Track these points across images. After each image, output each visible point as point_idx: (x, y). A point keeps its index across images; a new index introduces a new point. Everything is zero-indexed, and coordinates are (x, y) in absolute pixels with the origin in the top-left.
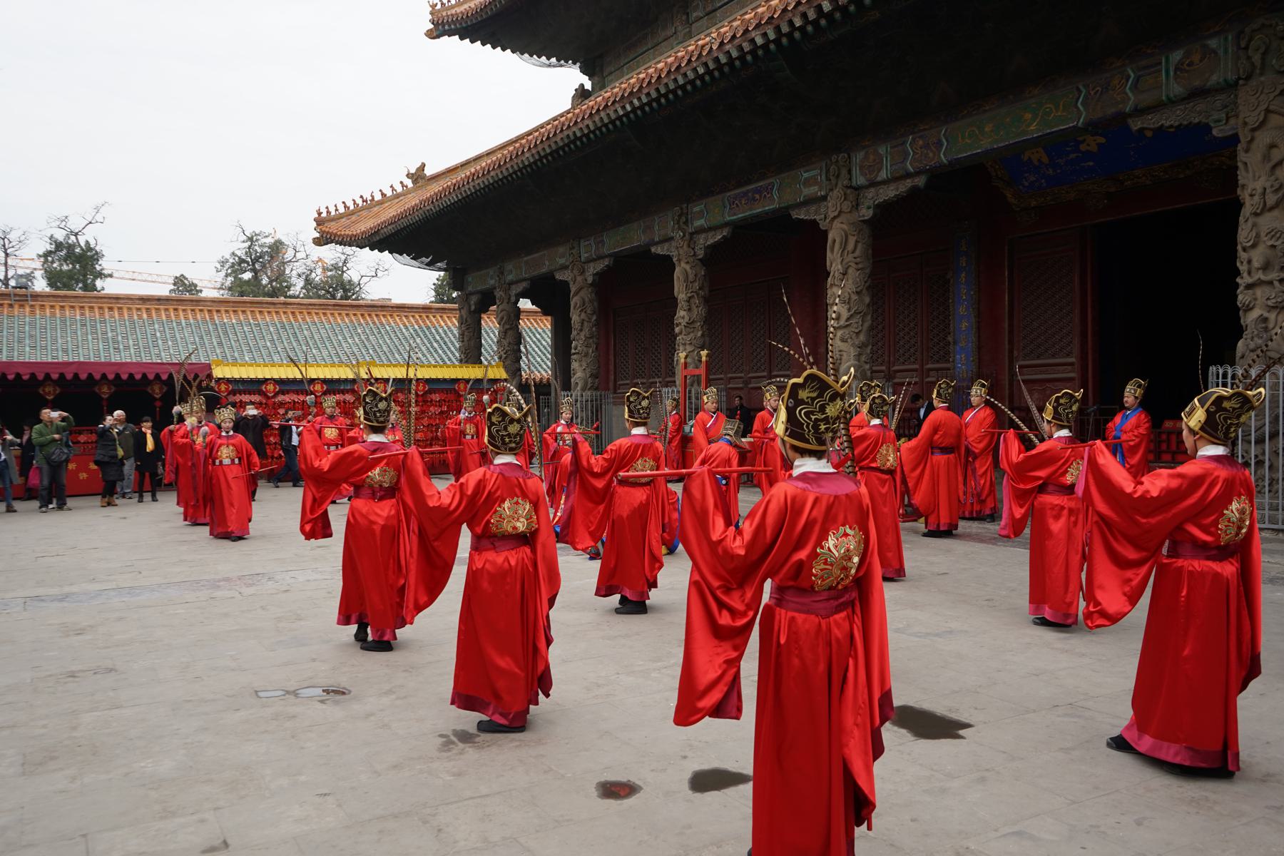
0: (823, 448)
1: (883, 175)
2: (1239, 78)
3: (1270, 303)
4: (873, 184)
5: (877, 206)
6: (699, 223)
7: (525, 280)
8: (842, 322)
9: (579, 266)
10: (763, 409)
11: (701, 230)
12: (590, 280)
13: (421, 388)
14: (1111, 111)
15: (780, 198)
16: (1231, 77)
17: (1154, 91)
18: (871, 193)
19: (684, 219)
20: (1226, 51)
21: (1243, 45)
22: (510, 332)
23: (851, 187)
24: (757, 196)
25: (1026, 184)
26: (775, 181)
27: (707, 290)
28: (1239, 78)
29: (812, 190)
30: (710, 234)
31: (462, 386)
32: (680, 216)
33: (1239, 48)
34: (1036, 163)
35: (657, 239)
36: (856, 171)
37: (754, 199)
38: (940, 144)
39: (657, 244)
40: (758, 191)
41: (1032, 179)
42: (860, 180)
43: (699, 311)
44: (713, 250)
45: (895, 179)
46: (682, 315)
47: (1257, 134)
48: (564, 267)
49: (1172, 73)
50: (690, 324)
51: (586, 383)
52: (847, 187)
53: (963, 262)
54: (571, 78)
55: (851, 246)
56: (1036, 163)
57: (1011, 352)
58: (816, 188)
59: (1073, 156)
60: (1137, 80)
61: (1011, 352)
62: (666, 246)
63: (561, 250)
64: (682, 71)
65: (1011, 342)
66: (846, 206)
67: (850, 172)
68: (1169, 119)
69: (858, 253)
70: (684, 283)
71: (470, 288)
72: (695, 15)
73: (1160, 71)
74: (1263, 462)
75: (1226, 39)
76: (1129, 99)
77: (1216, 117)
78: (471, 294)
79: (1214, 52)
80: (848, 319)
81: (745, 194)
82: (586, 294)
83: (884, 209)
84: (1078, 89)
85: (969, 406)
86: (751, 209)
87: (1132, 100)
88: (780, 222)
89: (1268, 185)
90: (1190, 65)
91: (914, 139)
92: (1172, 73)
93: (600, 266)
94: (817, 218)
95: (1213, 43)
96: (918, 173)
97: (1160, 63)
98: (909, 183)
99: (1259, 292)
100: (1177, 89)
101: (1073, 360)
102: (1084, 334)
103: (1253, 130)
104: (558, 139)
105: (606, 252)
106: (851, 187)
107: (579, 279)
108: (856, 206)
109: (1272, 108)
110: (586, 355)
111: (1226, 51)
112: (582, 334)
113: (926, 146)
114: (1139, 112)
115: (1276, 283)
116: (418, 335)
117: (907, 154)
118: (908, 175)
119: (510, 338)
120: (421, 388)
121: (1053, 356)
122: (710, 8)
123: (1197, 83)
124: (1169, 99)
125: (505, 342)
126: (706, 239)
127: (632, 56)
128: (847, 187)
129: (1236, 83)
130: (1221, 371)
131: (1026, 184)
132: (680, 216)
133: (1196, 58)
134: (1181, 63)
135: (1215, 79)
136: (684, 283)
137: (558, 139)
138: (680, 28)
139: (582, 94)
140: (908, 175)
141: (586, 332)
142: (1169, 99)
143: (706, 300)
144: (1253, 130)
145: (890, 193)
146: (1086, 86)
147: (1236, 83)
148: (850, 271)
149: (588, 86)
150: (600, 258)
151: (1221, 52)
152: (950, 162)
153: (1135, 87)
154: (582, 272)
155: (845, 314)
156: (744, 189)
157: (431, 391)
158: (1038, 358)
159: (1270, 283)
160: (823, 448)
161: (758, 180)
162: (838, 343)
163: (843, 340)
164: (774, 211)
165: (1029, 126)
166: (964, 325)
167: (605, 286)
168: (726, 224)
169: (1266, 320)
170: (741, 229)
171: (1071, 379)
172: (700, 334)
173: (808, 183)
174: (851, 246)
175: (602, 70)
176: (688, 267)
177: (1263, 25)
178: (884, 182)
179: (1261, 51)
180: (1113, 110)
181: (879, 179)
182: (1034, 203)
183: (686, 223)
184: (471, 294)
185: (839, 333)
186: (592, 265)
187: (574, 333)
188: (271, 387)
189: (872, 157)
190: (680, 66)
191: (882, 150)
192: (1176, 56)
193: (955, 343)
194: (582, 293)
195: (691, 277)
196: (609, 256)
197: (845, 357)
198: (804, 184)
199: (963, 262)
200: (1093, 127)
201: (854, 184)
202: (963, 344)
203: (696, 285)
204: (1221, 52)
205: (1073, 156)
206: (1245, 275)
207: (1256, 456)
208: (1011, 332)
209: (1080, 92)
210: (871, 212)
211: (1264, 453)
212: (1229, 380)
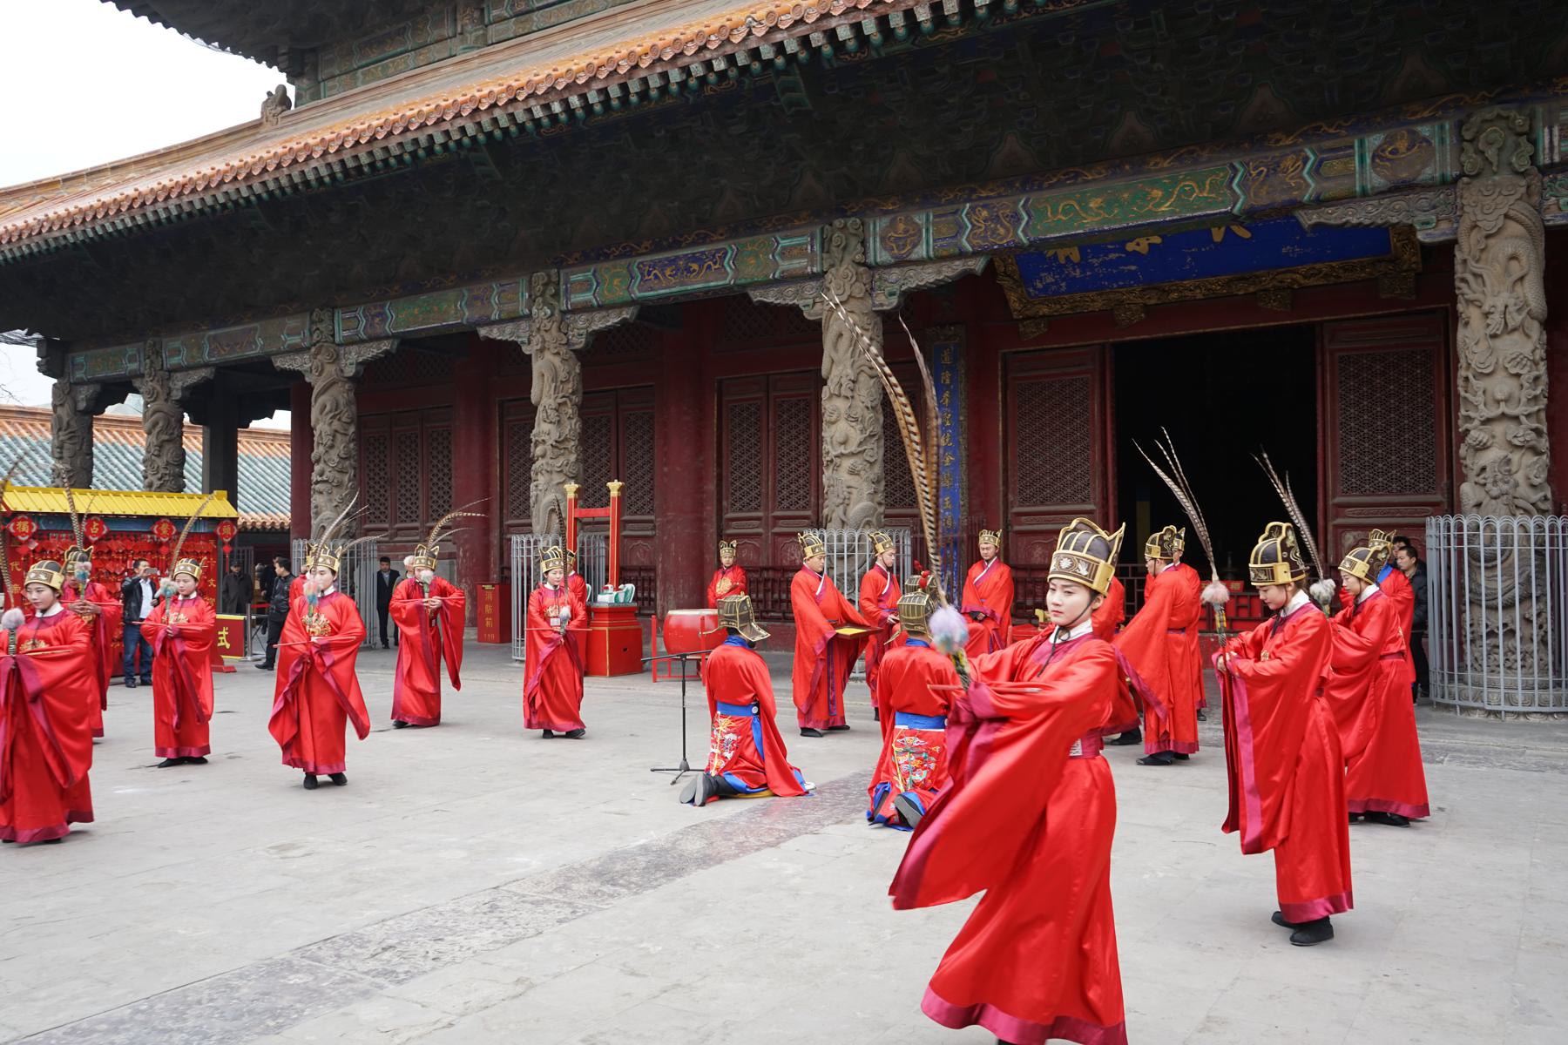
1: (921, 251)
3: (1516, 442)
4: (901, 263)
6: (579, 298)
7: (206, 365)
8: (852, 448)
9: (331, 353)
10: (800, 568)
12: (350, 371)
13: (95, 530)
14: (1281, 198)
15: (736, 270)
16: (1451, 172)
17: (1347, 180)
18: (895, 274)
20: (1442, 141)
21: (1468, 136)
22: (168, 447)
23: (864, 264)
24: (695, 266)
25: (1040, 286)
26: (731, 248)
28: (1463, 175)
29: (798, 264)
30: (597, 316)
31: (164, 528)
32: (546, 285)
33: (1462, 139)
34: (1062, 260)
38: (1016, 218)
39: (492, 323)
40: (694, 258)
41: (1050, 279)
42: (884, 257)
43: (572, 426)
44: (600, 339)
46: (544, 430)
47: (1492, 241)
48: (297, 350)
49: (1368, 160)
52: (859, 264)
54: (272, 78)
57: (1005, 495)
58: (804, 262)
60: (1319, 164)
61: (1005, 495)
62: (509, 328)
63: (291, 323)
64: (681, 62)
65: (1006, 483)
66: (859, 290)
67: (863, 243)
70: (550, 385)
71: (79, 375)
72: (495, 13)
73: (1352, 155)
74: (1513, 632)
75: (1442, 127)
76: (1308, 185)
77: (1422, 217)
78: (81, 383)
79: (1425, 140)
80: (860, 444)
82: (341, 393)
85: (975, 557)
86: (683, 284)
88: (730, 307)
89: (1511, 302)
91: (972, 209)
92: (1368, 160)
93: (372, 351)
94: (801, 303)
95: (1425, 130)
96: (975, 254)
97: (1352, 147)
98: (958, 266)
99: (1499, 429)
100: (1376, 180)
102: (1104, 475)
103: (1488, 237)
104: (392, 144)
105: (388, 330)
106: (864, 264)
107: (330, 369)
108: (870, 292)
109: (1512, 213)
110: (340, 485)
111: (1442, 141)
112: (334, 454)
113: (996, 219)
114: (1319, 202)
115: (1523, 418)
116: (1474, 556)
117: (962, 227)
118: (962, 255)
119: (168, 454)
120: (95, 530)
121: (1063, 502)
122: (522, 7)
124: (1364, 189)
125: (160, 462)
126: (591, 322)
127: (374, 58)
129: (1455, 181)
130: (1452, 521)
131: (1040, 286)
133: (1402, 145)
134: (1381, 148)
135: (1428, 173)
136: (550, 385)
137: (392, 144)
138: (469, 28)
139: (278, 101)
140: (962, 255)
141: (340, 448)
142: (1364, 189)
143: (583, 411)
145: (927, 276)
146: (1245, 165)
147: (1455, 181)
149: (291, 92)
151: (1436, 142)
152: (1031, 244)
153: (1316, 171)
154: (336, 359)
157: (111, 536)
159: (1516, 418)
161: (695, 243)
162: (843, 475)
163: (852, 472)
165: (1159, 205)
167: (371, 386)
168: (633, 302)
169: (1508, 462)
170: (650, 311)
172: (573, 458)
173: (786, 253)
176: (557, 361)
177: (1499, 116)
178: (921, 262)
179: (1497, 146)
180: (1285, 197)
181: (914, 256)
182: (1045, 310)
183: (556, 295)
184: (81, 383)
185: (847, 463)
186: (354, 348)
188: (23, 526)
189: (902, 227)
190: (636, 66)
191: (919, 219)
192: (1374, 140)
195: (562, 376)
196: (394, 336)
197: (854, 496)
198: (782, 254)
201: (871, 260)
203: (569, 387)
204: (1436, 142)
205: (1113, 256)
206: (1482, 407)
207: (1505, 625)
208: (1005, 470)
209: (1236, 171)
210: (894, 301)
211: (1513, 622)
212: (1453, 533)
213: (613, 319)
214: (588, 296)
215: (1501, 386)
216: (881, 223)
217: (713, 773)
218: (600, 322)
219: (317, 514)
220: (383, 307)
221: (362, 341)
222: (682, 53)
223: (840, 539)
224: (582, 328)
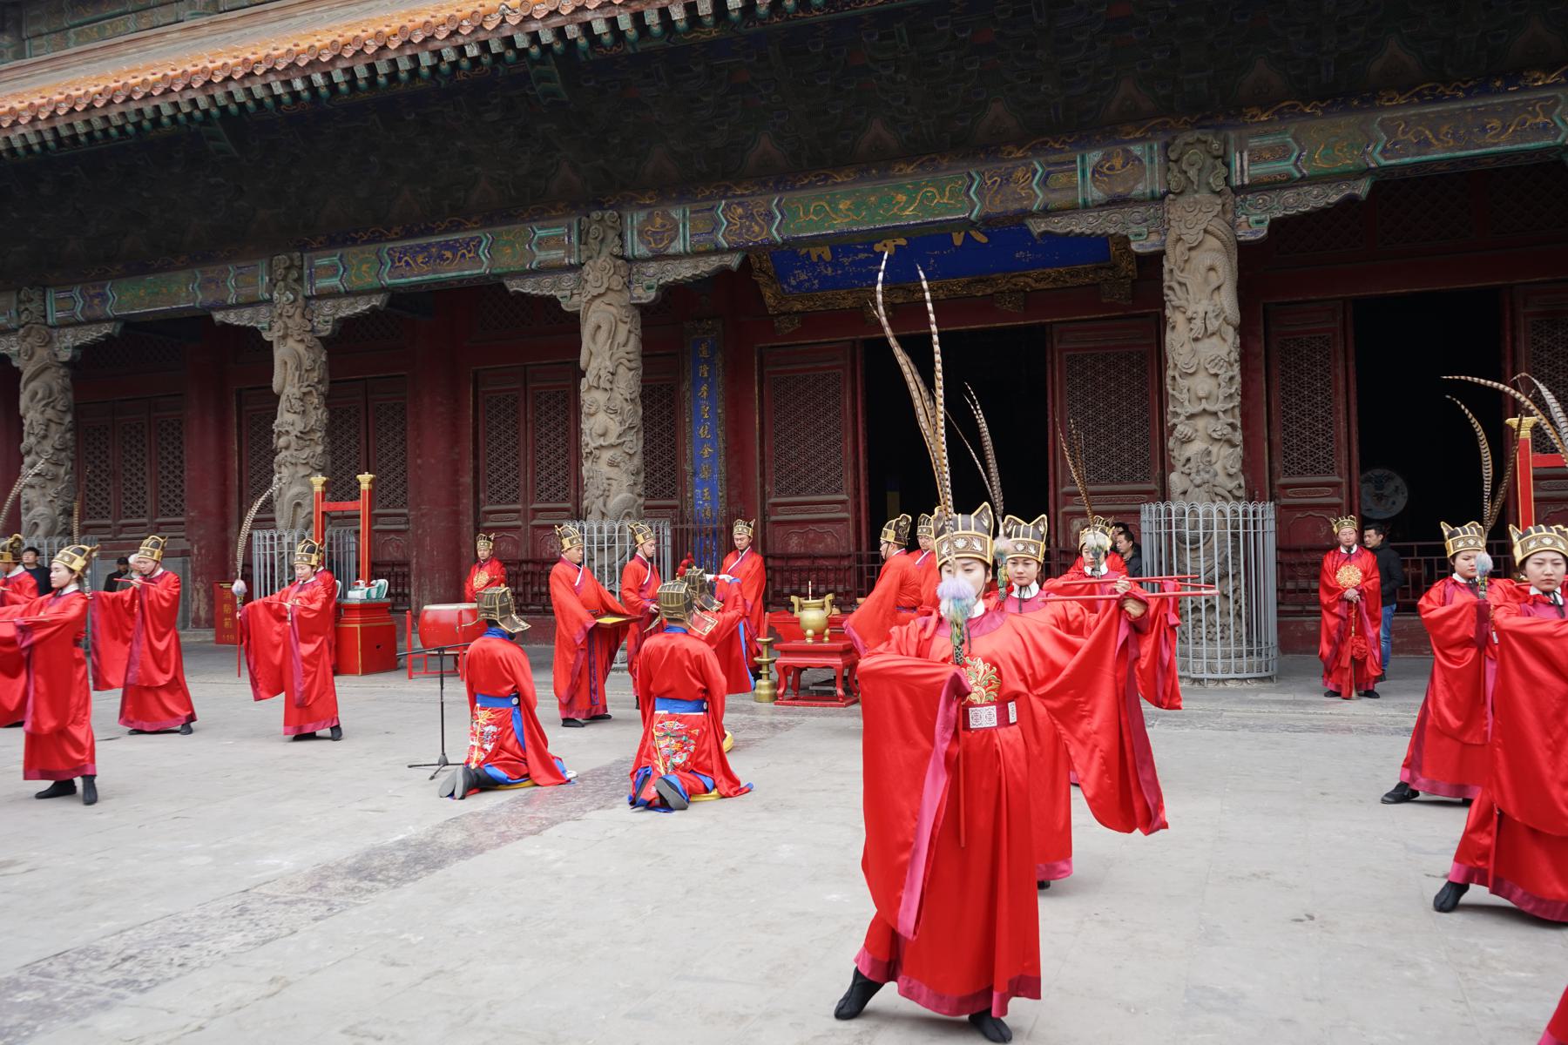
0: (1171, 600)
1: (678, 246)
2: (1169, 192)
3: (1215, 435)
4: (659, 257)
5: (661, 287)
6: (324, 283)
10: (559, 560)
11: (332, 294)
12: (65, 356)
15: (492, 259)
16: (1159, 189)
18: (652, 268)
19: (294, 274)
20: (1152, 161)
24: (448, 254)
25: (793, 283)
26: (486, 237)
27: (327, 382)
28: (1169, 192)
29: (555, 255)
30: (345, 302)
32: (288, 269)
33: (1168, 159)
34: (815, 259)
35: (232, 300)
36: (632, 238)
37: (441, 257)
41: (804, 277)
45: (697, 254)
46: (287, 420)
47: (1193, 253)
49: (1089, 175)
50: (303, 435)
51: (54, 523)
52: (617, 257)
53: (704, 370)
55: (621, 338)
56: (815, 259)
57: (763, 486)
58: (561, 253)
59: (862, 256)
61: (763, 486)
64: (432, 46)
65: (763, 475)
66: (617, 282)
67: (621, 236)
68: (1080, 225)
69: (630, 348)
70: (294, 372)
75: (1151, 148)
77: (1135, 229)
80: (620, 436)
81: (424, 248)
82: (56, 380)
83: (672, 293)
84: (970, 176)
86: (435, 272)
87: (1040, 199)
89: (1210, 309)
90: (1111, 168)
92: (1089, 175)
93: (90, 335)
94: (559, 294)
95: (1137, 150)
96: (731, 250)
98: (714, 262)
99: (1201, 423)
100: (1096, 194)
101: (568, 505)
103: (1190, 249)
104: (113, 113)
106: (622, 257)
108: (628, 285)
110: (55, 478)
111: (1152, 161)
114: (1047, 212)
116: (1181, 539)
118: (718, 251)
121: (818, 492)
123: (1120, 190)
126: (338, 308)
128: (617, 257)
131: (793, 283)
132: (288, 269)
133: (1118, 162)
135: (1140, 189)
136: (294, 372)
140: (718, 251)
141: (55, 437)
144: (1190, 249)
145: (684, 271)
147: (1163, 197)
148: (621, 370)
150: (98, 321)
151: (1146, 161)
152: (785, 242)
153: (1044, 182)
154: (48, 343)
155: (615, 429)
156: (422, 241)
158: (798, 494)
159: (1215, 414)
160: (1171, 600)
162: (603, 467)
163: (612, 464)
164: (479, 277)
166: (707, 451)
168: (383, 289)
169: (1209, 453)
171: (1338, 506)
172: (319, 449)
173: (542, 243)
174: (621, 338)
175: (18, 26)
176: (301, 348)
178: (677, 257)
180: (1017, 206)
181: (671, 251)
182: (799, 307)
185: (606, 455)
186: (70, 332)
187: (29, 441)
189: (659, 221)
191: (676, 214)
192: (1094, 157)
193: (695, 474)
194: (46, 377)
195: (307, 364)
196: (116, 319)
198: (539, 245)
199: (704, 370)
200: (987, 222)
201: (628, 253)
202: (705, 475)
204: (1146, 161)
205: (862, 256)
208: (762, 462)
209: (972, 179)
210: (652, 294)
213: (362, 306)
214: (335, 282)
215: (1202, 385)
216: (639, 217)
217: (473, 765)
218: (348, 309)
219: (28, 510)
220: (103, 287)
221: (79, 324)
222: (433, 37)
223: (600, 531)
224: (328, 315)
